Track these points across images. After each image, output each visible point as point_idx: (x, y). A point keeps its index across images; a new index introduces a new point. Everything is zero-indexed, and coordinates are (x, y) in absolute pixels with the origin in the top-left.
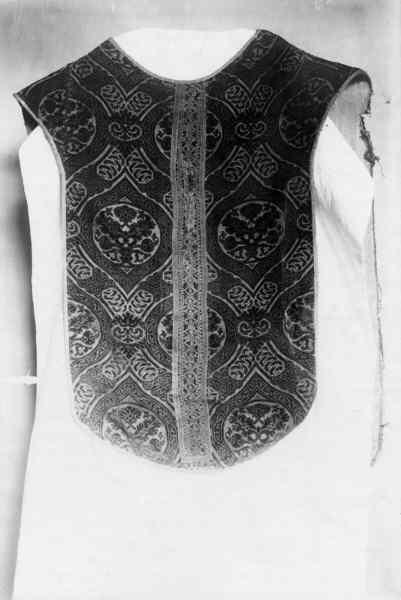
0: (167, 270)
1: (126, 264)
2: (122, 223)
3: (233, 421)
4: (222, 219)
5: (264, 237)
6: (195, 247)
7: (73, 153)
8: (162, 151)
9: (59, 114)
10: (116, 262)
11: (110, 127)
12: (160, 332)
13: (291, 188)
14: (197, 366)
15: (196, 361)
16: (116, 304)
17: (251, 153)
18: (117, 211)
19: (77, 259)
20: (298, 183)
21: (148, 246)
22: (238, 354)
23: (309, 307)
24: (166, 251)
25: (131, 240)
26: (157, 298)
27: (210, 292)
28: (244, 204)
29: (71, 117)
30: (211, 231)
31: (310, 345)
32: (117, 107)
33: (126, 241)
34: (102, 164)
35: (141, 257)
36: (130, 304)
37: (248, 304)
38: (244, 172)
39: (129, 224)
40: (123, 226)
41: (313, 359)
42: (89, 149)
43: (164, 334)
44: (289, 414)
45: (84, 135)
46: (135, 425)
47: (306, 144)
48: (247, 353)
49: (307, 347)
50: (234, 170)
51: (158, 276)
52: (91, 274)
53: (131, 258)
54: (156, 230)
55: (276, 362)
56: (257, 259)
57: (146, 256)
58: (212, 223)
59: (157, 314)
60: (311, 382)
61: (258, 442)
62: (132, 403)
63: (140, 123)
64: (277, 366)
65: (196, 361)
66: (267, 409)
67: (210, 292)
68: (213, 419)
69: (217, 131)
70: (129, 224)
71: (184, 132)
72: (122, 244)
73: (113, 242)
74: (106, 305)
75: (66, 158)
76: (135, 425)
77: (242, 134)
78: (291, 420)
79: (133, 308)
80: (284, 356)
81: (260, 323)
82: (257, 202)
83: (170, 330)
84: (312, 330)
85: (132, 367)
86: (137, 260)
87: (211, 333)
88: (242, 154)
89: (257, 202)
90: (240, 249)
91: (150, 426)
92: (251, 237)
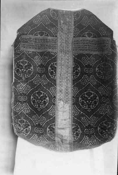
5: (93, 102)
9: (27, 70)
11: (85, 70)
16: (86, 122)
18: (87, 94)
19: (26, 107)
22: (33, 137)
25: (91, 102)
28: (87, 92)
33: (89, 102)
34: (35, 80)
40: (88, 98)
42: (78, 77)
52: (30, 111)
53: (40, 106)
56: (41, 109)
70: (90, 97)
72: (88, 103)
73: (36, 101)
81: (91, 130)
90: (86, 105)
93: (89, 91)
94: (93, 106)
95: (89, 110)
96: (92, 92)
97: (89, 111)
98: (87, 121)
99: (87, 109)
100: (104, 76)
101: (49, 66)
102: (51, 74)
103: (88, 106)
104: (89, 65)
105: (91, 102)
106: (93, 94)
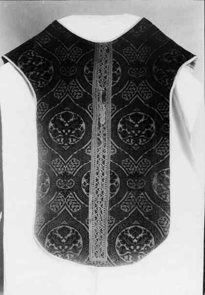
0: (88, 147)
1: (66, 144)
2: (65, 122)
3: (120, 238)
4: (121, 120)
6: (105, 135)
7: (41, 87)
8: (88, 81)
10: (60, 143)
12: (83, 183)
13: (160, 108)
14: (107, 64)
15: (102, 200)
17: (137, 85)
18: (63, 116)
20: (163, 105)
21: (78, 134)
23: (168, 176)
24: (88, 135)
25: (69, 131)
26: (82, 163)
27: (112, 161)
29: (38, 66)
30: (114, 126)
31: (168, 198)
32: (64, 58)
35: (74, 140)
36: (69, 54)
37: (133, 169)
38: (133, 95)
39: (69, 122)
41: (169, 205)
43: (85, 183)
44: (152, 236)
45: (47, 76)
46: (66, 237)
47: (168, 84)
48: (132, 197)
49: (166, 199)
50: (127, 94)
51: (83, 151)
54: (83, 125)
55: (148, 205)
57: (77, 140)
58: (114, 122)
59: (82, 171)
60: (167, 220)
61: (135, 251)
62: (66, 225)
63: (73, 178)
64: (149, 207)
65: (102, 200)
66: (140, 231)
67: (112, 161)
68: (110, 237)
69: (118, 71)
71: (100, 70)
74: (54, 168)
75: (37, 90)
76: (66, 237)
77: (132, 74)
78: (152, 241)
79: (68, 169)
80: (152, 202)
82: (139, 227)
83: (88, 181)
84: (169, 189)
85: (67, 203)
86: (72, 142)
87: (111, 184)
88: (132, 85)
89: (139, 227)
91: (74, 239)
92: (136, 132)
93: (137, 225)
94: (43, 83)
95: (67, 146)
96: (142, 228)
97: (66, 148)
98: (61, 166)
99: (63, 145)
100: (132, 140)
101: (82, 177)
102: (121, 253)
103: (65, 139)
104: (68, 61)
105: (69, 131)
106: (143, 231)
